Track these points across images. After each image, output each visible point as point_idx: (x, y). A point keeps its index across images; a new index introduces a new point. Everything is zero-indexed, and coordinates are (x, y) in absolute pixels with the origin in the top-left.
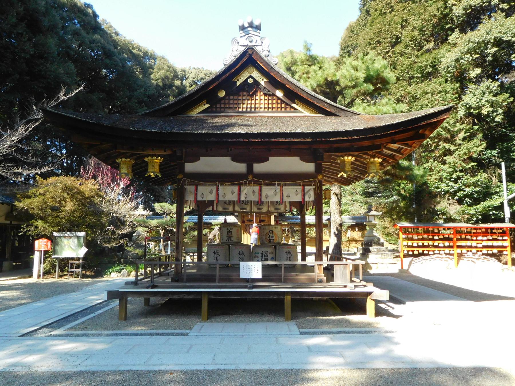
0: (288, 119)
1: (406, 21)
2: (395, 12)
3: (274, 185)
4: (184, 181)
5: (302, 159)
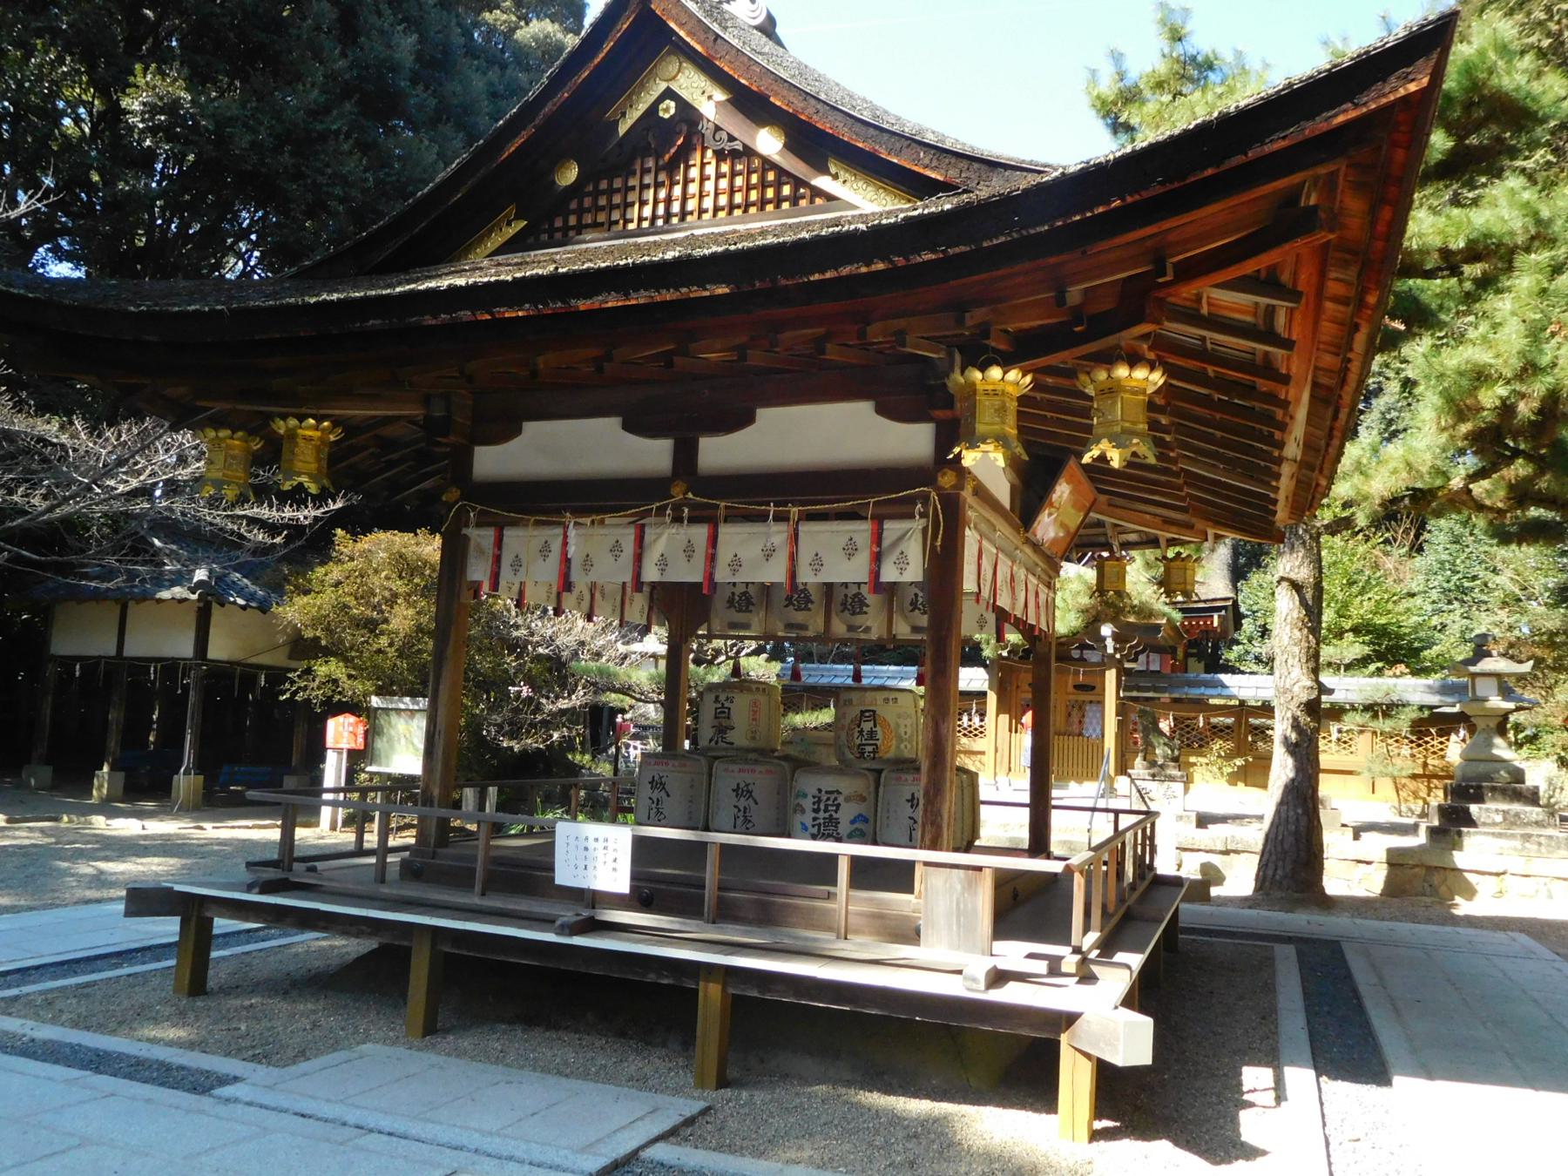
3: (762, 518)
4: (463, 512)
5: (883, 410)
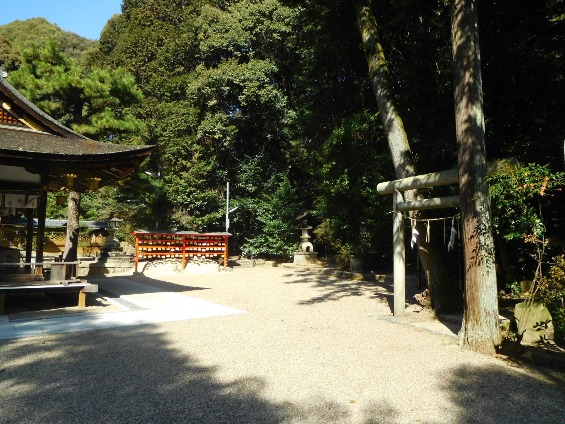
0: (13, 133)
1: (162, 40)
2: (154, 27)
5: (27, 170)
